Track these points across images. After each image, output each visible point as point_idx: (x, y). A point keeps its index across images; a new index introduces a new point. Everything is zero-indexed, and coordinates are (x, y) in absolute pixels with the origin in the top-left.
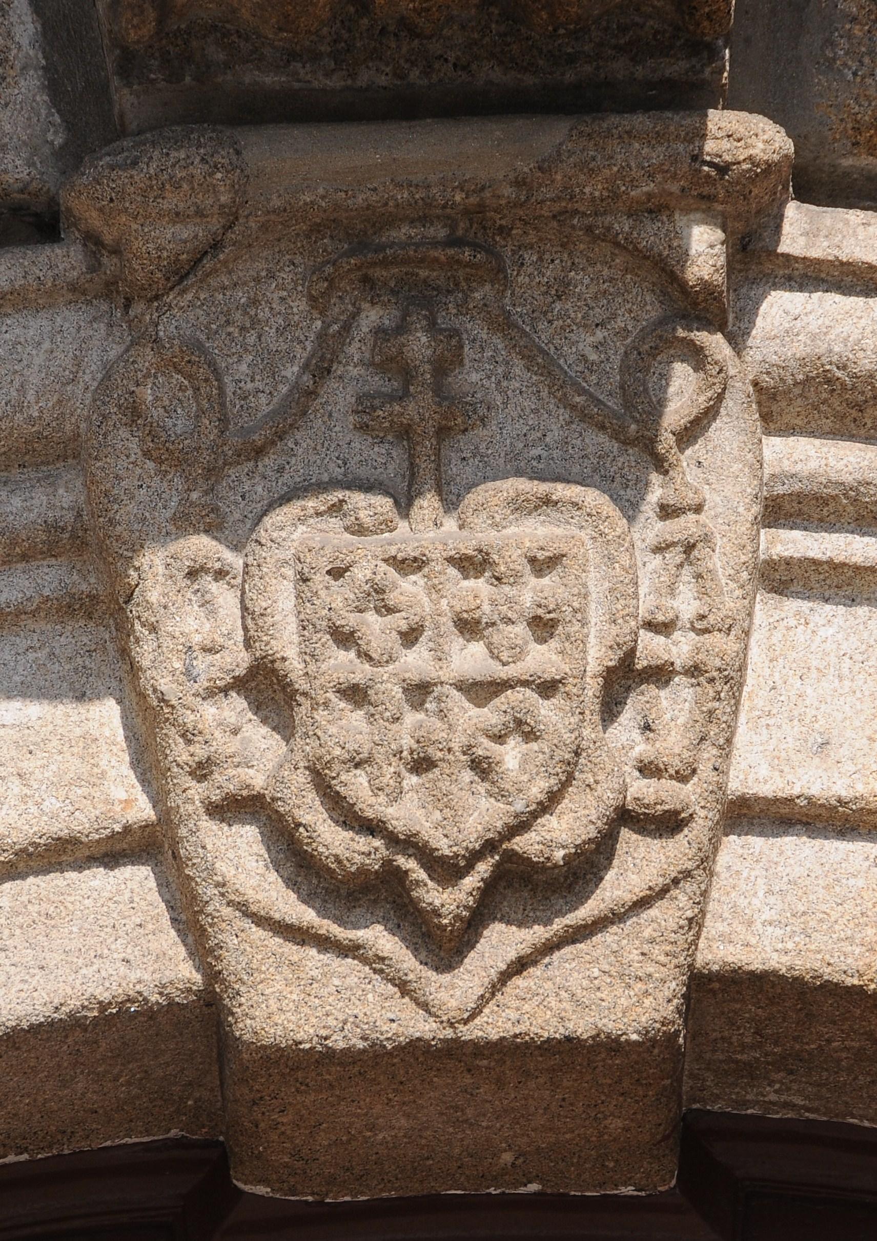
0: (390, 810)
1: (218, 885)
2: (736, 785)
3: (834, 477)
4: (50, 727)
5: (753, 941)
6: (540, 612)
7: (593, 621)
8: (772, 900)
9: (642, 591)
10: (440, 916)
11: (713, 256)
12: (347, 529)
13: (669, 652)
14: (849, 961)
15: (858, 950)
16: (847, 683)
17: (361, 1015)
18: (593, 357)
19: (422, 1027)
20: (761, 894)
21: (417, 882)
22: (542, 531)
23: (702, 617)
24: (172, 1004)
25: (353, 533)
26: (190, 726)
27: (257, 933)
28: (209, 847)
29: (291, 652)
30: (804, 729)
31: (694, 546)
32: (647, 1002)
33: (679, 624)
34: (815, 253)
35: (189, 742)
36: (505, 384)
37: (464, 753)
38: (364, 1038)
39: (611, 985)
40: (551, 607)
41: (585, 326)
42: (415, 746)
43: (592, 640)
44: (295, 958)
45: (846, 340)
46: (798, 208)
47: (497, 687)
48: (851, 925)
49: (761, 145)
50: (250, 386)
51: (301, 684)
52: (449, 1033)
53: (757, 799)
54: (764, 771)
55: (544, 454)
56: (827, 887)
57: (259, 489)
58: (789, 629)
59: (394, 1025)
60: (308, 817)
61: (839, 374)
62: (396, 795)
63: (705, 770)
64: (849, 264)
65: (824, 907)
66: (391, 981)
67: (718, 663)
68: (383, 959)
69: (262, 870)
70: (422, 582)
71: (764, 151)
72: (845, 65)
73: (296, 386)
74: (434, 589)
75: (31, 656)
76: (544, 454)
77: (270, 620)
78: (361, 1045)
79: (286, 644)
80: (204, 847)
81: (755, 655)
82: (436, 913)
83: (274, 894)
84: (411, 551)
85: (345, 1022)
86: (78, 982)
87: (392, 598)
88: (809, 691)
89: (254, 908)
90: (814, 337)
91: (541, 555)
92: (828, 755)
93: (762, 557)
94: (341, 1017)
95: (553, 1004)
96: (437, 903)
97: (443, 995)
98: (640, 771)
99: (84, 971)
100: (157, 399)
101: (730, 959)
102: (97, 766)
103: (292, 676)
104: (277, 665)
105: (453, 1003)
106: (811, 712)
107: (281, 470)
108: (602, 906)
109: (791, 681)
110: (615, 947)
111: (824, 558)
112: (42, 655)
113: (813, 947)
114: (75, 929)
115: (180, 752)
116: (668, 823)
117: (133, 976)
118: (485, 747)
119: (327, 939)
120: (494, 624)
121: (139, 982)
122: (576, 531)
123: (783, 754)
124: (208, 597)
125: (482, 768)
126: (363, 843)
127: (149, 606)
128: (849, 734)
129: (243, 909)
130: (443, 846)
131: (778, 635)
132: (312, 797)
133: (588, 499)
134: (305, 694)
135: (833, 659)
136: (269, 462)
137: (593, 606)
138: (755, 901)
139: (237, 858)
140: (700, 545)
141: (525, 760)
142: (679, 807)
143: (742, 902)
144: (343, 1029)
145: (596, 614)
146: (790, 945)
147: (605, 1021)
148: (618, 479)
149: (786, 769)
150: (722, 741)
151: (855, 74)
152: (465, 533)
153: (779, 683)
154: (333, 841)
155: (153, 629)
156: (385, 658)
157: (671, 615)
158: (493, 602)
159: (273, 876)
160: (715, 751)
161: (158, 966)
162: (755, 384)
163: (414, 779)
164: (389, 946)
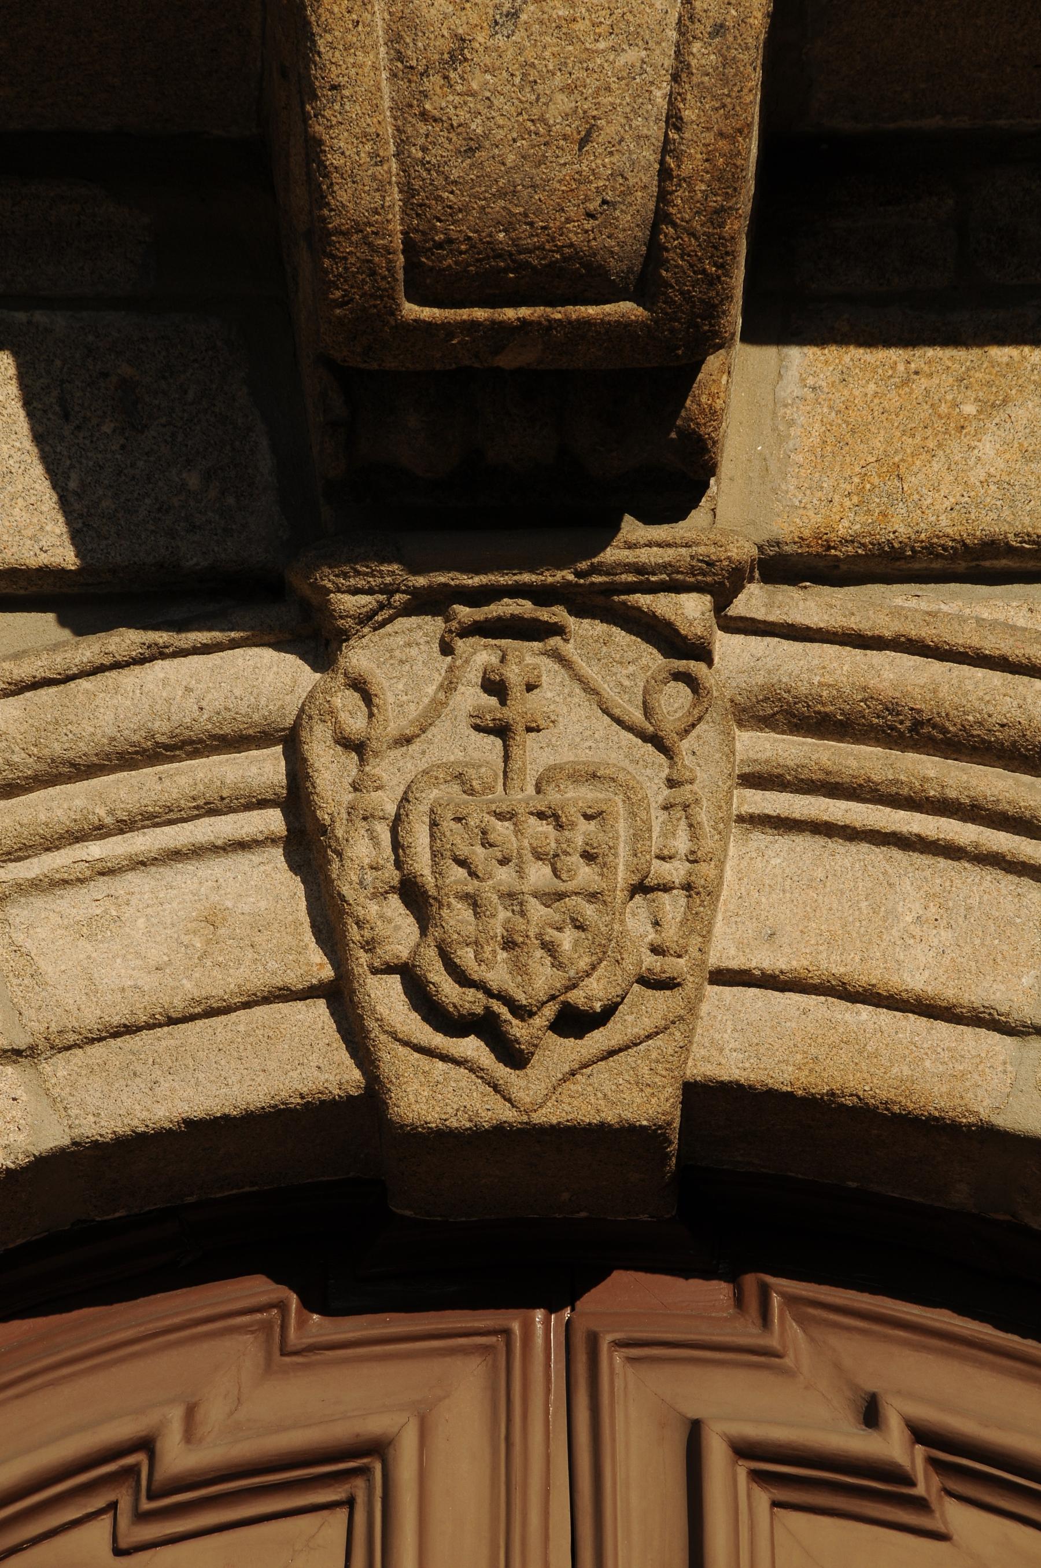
0: (488, 975)
1: (377, 1020)
2: (714, 960)
3: (781, 761)
4: (273, 915)
5: (723, 1062)
6: (588, 848)
7: (622, 854)
8: (736, 1035)
9: (655, 835)
10: (519, 1043)
11: (704, 620)
12: (464, 792)
13: (671, 875)
14: (785, 1076)
15: (790, 1069)
16: (788, 895)
17: (468, 1106)
18: (626, 683)
19: (508, 1114)
20: (729, 1031)
21: (505, 1021)
22: (590, 795)
23: (693, 852)
24: (350, 1097)
25: (469, 795)
26: (361, 918)
27: (403, 1051)
28: (372, 996)
29: (427, 872)
30: (760, 925)
31: (688, 806)
32: (653, 1101)
33: (678, 857)
34: (771, 618)
35: (359, 927)
36: (569, 699)
37: (537, 939)
38: (14, 1163)
39: (630, 1089)
40: (595, 845)
41: (621, 663)
42: (505, 934)
43: (621, 867)
44: (427, 1069)
45: (790, 674)
46: (761, 588)
47: (560, 896)
48: (787, 1052)
49: (735, 550)
50: (405, 698)
51: (432, 892)
52: (525, 1118)
53: (728, 970)
54: (733, 952)
55: (594, 745)
56: (772, 1027)
57: (409, 765)
58: (751, 859)
59: (490, 1113)
60: (436, 978)
61: (785, 695)
62: (490, 965)
63: (693, 951)
64: (792, 625)
65: (770, 1041)
66: (489, 1084)
67: (703, 882)
68: (482, 1070)
69: (406, 1011)
70: (512, 827)
71: (737, 554)
72: (794, 495)
73: (433, 700)
74: (518, 832)
75: (262, 868)
76: (594, 745)
77: (413, 850)
78: (468, 1125)
79: (422, 864)
80: (369, 996)
81: (729, 874)
82: (517, 1041)
83: (414, 1027)
84: (504, 808)
85: (457, 1110)
86: (287, 1081)
87: (492, 837)
88: (764, 900)
89: (400, 1036)
90: (769, 672)
91: (589, 812)
92: (774, 942)
93: (735, 813)
94: (455, 1107)
95: (593, 1101)
96: (518, 1035)
97: (521, 1094)
98: (652, 951)
99: (291, 1073)
100: (344, 706)
101: (708, 1073)
102: (302, 941)
103: (428, 887)
104: (419, 879)
105: (528, 1100)
106: (764, 914)
107: (424, 753)
108: (625, 1038)
109: (752, 893)
110: (634, 1065)
111: (775, 814)
112: (268, 868)
113: (762, 1066)
114: (286, 1046)
115: (354, 933)
116: (668, 984)
117: (323, 1078)
118: (551, 934)
119: (447, 1056)
120: (558, 855)
121: (327, 1081)
122: (612, 795)
123: (746, 941)
124: (375, 834)
125: (550, 948)
126: (471, 993)
127: (337, 840)
128: (788, 928)
129: (395, 1037)
130: (522, 998)
131: (744, 863)
132: (439, 965)
133: (620, 776)
134: (435, 899)
135: (780, 880)
136: (415, 748)
137: (622, 845)
138: (726, 1036)
139: (386, 1000)
140: (693, 806)
141: (576, 943)
142: (676, 975)
143: (717, 1036)
144: (456, 1115)
145: (623, 850)
146: (747, 1065)
147: (626, 1112)
148: (641, 762)
149: (747, 951)
150: (704, 933)
151: (800, 502)
152: (541, 796)
153: (744, 894)
154: (449, 991)
155: (340, 854)
156: (487, 876)
157: (673, 851)
158: (557, 841)
159: (415, 1015)
160: (700, 939)
161: (335, 1073)
162: (732, 701)
163: (505, 955)
164: (487, 1062)
